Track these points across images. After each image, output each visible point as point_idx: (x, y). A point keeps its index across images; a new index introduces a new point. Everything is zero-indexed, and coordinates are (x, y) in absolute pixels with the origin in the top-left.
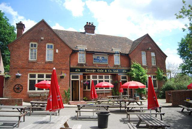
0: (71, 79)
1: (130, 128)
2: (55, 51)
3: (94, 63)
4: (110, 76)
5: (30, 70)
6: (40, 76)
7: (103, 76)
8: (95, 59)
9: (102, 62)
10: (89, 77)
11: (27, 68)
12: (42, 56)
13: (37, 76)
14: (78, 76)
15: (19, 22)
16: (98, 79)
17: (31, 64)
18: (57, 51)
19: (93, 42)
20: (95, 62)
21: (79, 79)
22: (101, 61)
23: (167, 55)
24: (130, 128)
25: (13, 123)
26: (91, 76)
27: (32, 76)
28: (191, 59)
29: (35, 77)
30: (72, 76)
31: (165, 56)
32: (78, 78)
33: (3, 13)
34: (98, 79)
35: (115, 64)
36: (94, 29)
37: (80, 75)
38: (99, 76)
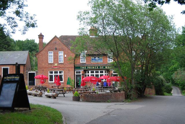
0: (76, 74)
2: (64, 56)
4: (104, 71)
5: (49, 69)
10: (88, 73)
11: (48, 68)
12: (56, 60)
13: (58, 72)
16: (99, 74)
18: (65, 56)
26: (90, 71)
27: (52, 73)
28: (1, 44)
29: (94, 73)
30: (76, 72)
32: (80, 73)
33: (178, 3)
34: (99, 74)
35: (49, 62)
37: (82, 72)
38: (100, 71)
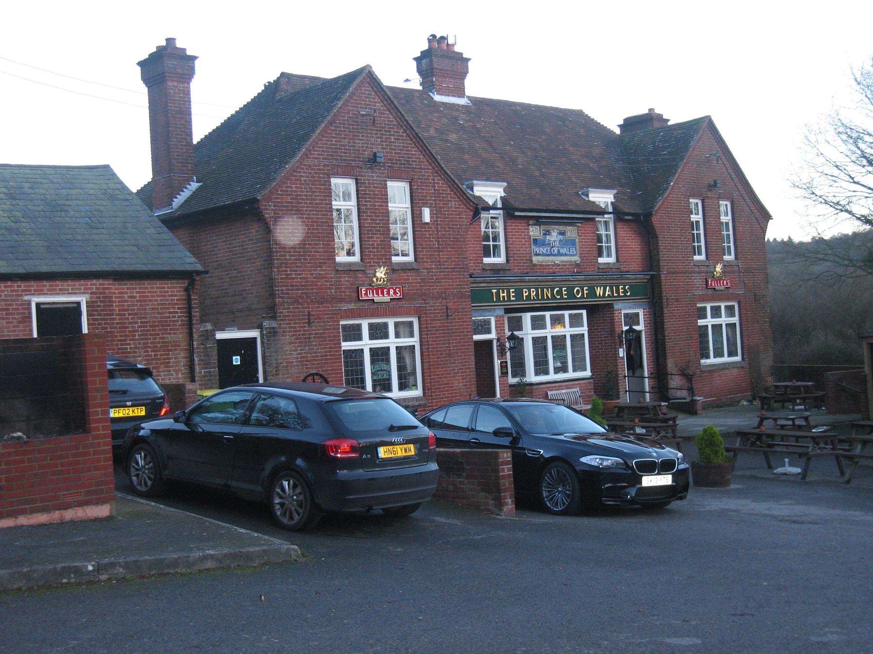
1: (854, 191)
3: (535, 259)
6: (378, 332)
7: (544, 316)
8: (536, 241)
9: (559, 254)
14: (488, 322)
15: (164, 43)
17: (345, 279)
19: (752, 220)
20: (537, 255)
21: (493, 336)
22: (556, 251)
23: (771, 212)
24: (854, 191)
25: (415, 504)
26: (527, 318)
31: (767, 216)
32: (489, 332)
36: (464, 73)
